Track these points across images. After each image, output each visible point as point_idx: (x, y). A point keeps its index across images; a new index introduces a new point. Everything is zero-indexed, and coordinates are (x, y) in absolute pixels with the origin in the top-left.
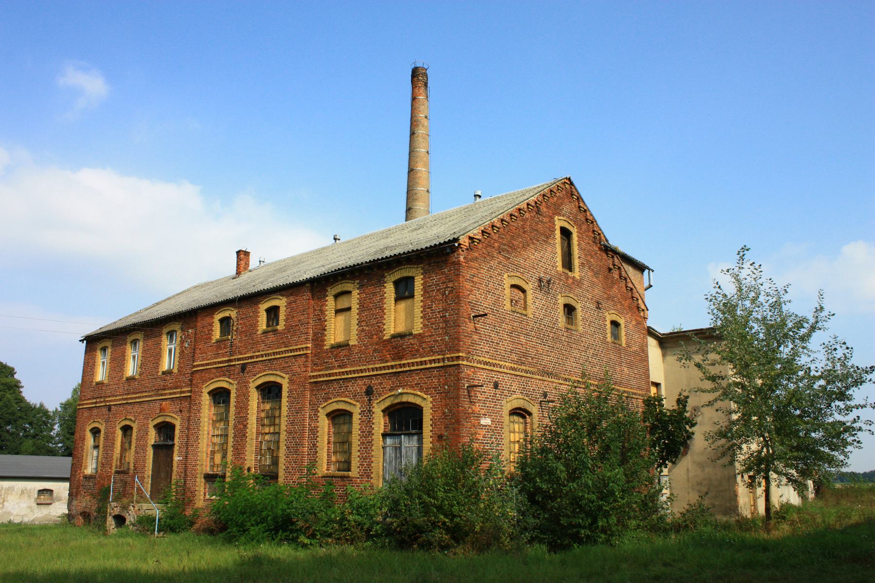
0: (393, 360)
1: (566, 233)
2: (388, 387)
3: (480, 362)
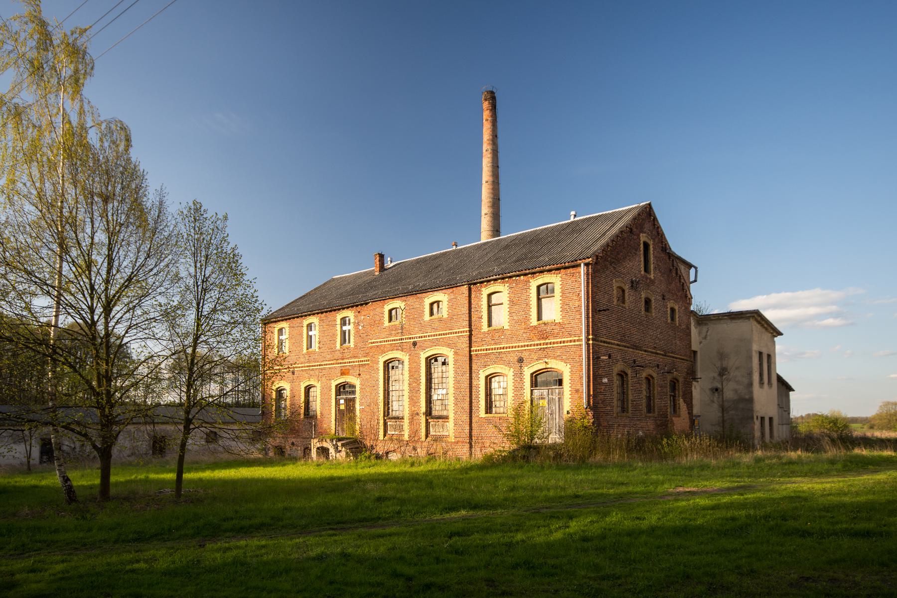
0: (539, 339)
1: (646, 246)
2: (535, 358)
3: (601, 341)
